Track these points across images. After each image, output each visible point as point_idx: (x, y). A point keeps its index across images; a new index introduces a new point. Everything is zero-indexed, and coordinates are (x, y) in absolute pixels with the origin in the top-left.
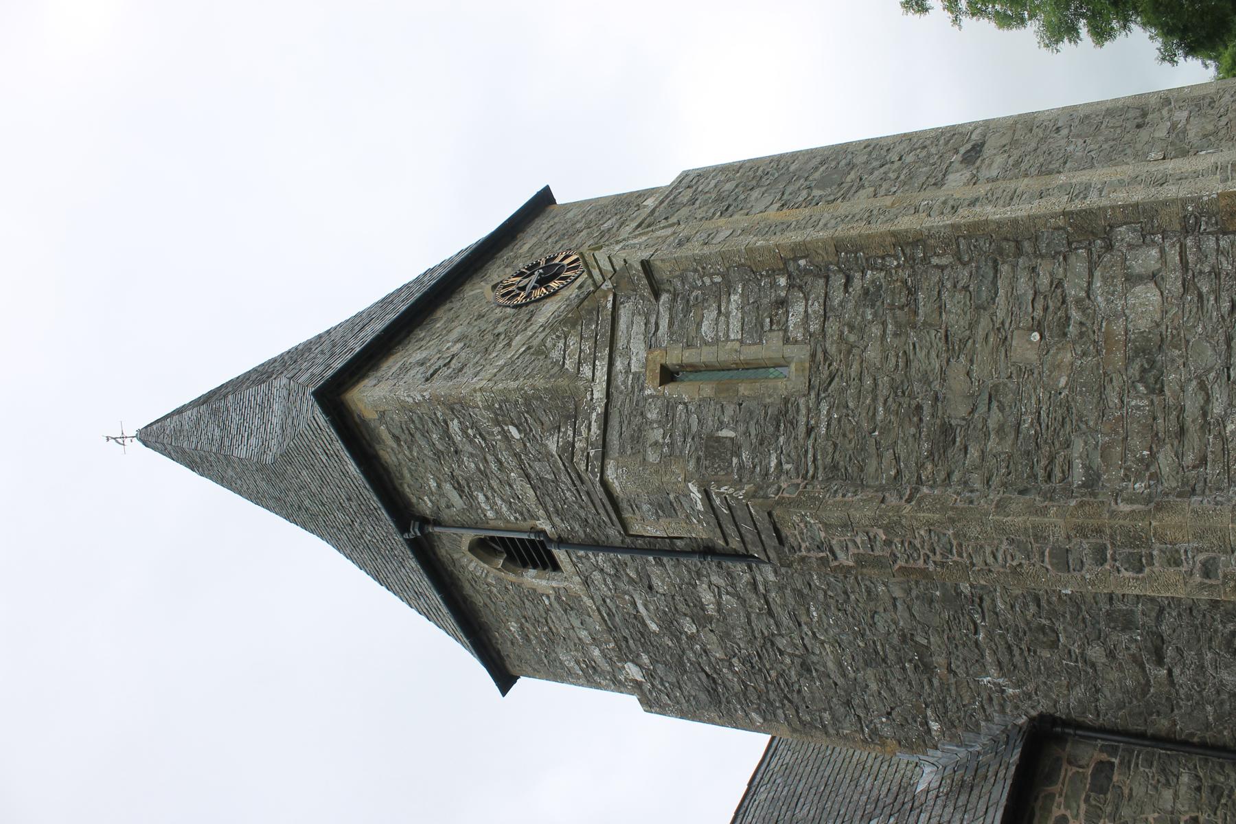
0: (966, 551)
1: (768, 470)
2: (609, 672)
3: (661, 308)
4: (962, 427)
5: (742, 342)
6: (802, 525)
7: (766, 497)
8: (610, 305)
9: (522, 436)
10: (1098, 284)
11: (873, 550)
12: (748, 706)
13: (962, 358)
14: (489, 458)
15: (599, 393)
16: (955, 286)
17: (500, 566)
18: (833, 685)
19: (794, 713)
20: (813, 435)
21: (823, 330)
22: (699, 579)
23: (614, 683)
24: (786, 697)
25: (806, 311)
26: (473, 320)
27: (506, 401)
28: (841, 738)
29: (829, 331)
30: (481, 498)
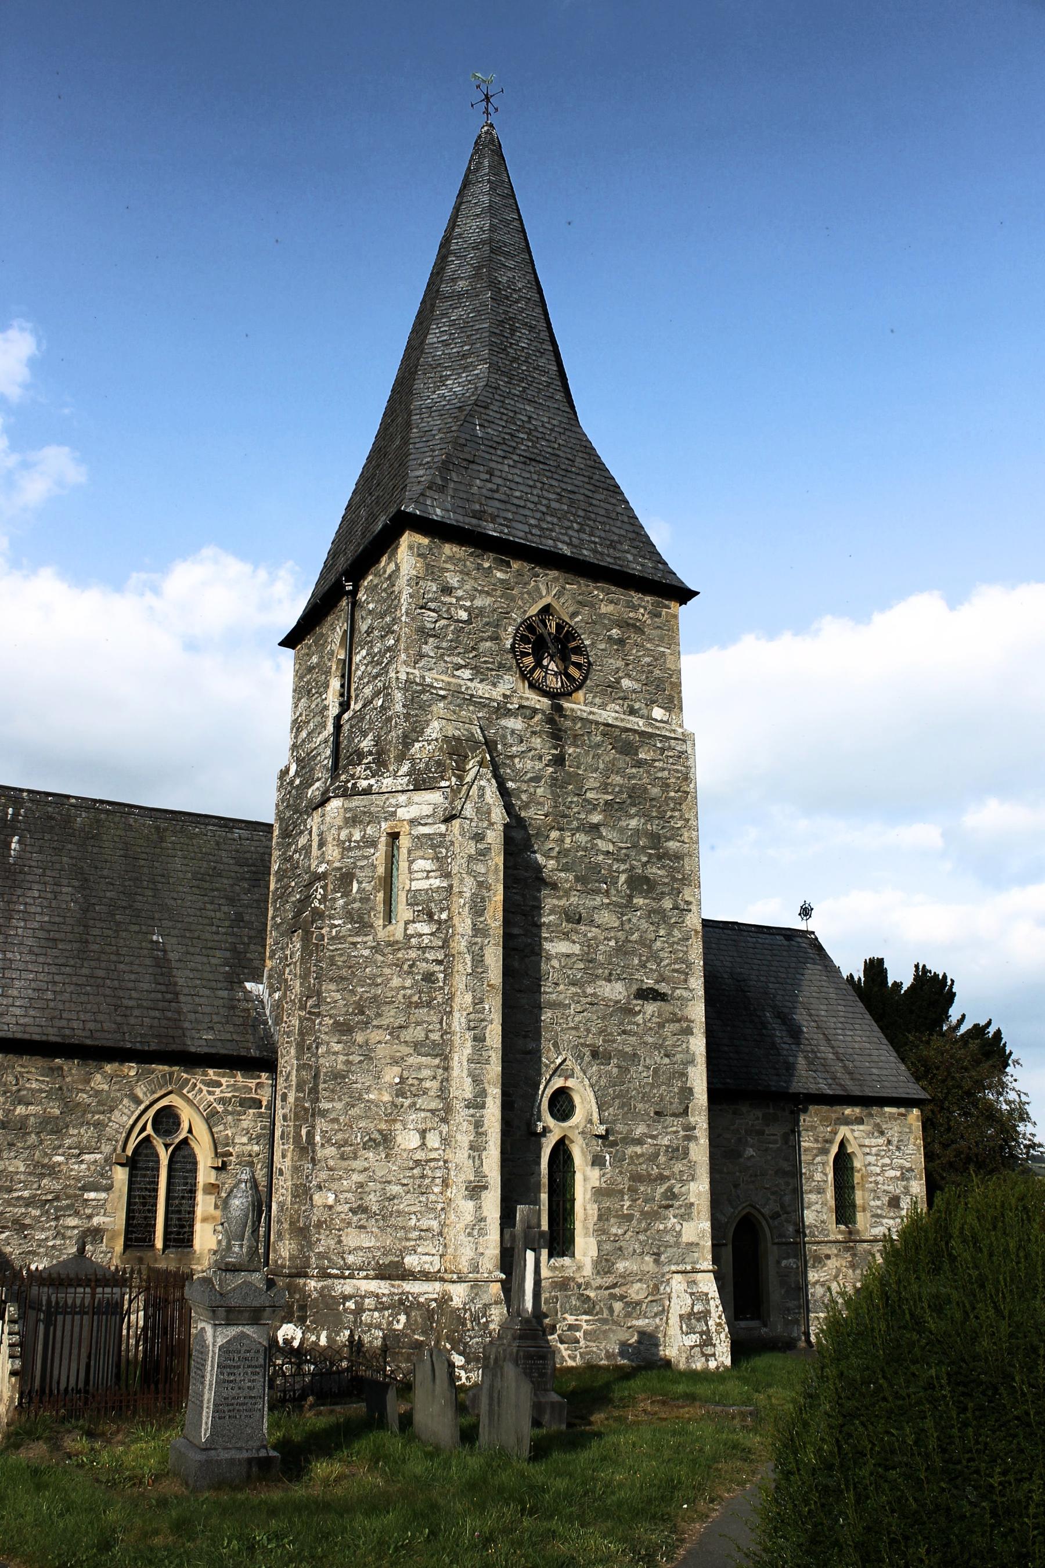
7: (312, 923)
10: (423, 1114)
13: (388, 1037)
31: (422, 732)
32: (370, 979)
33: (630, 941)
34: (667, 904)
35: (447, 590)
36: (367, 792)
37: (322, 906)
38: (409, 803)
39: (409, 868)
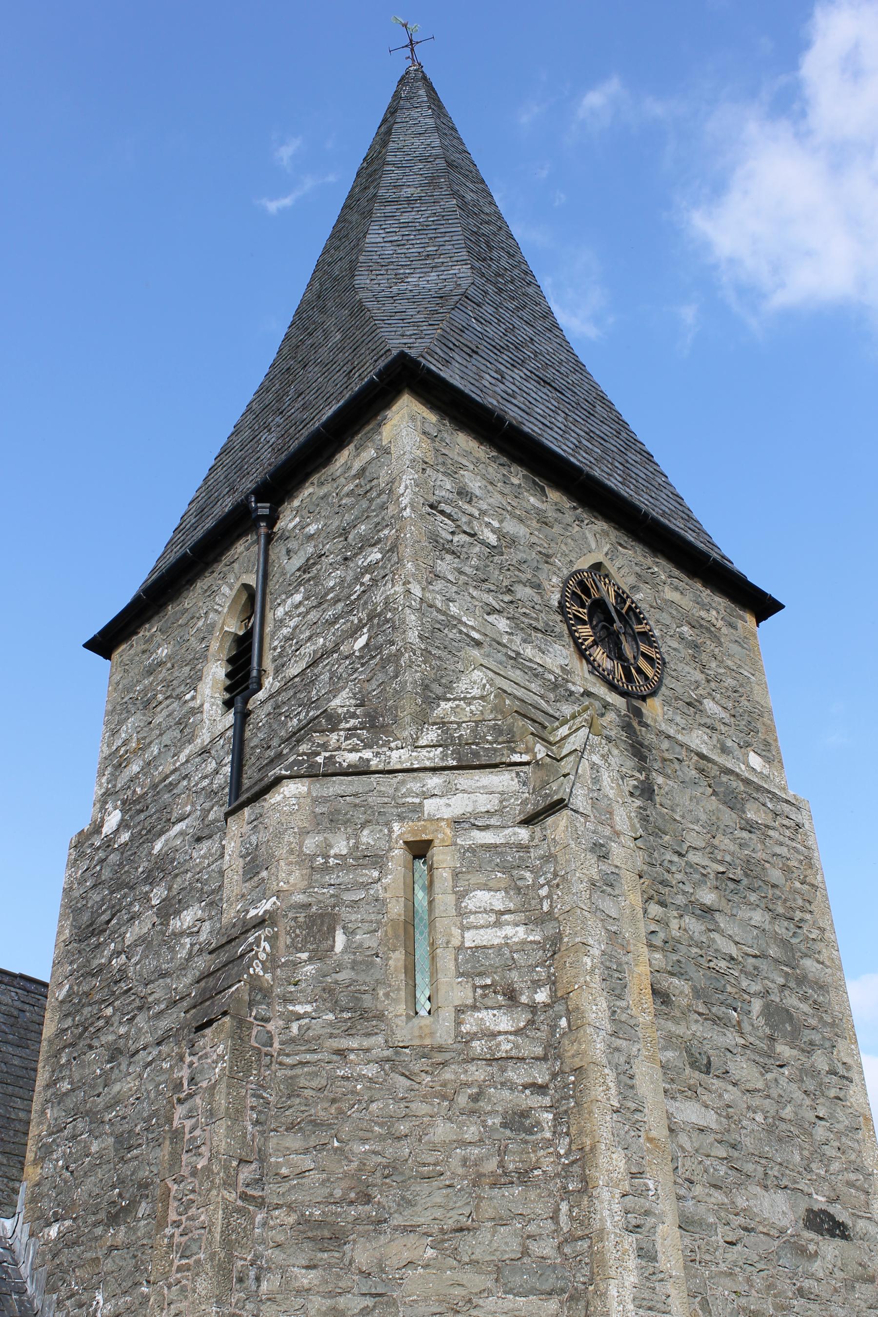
0: (182, 1277)
1: (292, 1002)
2: (114, 786)
3: (511, 829)
4: (341, 1259)
5: (460, 949)
6: (215, 1057)
7: (251, 1004)
8: (516, 758)
9: (357, 654)
11: (187, 1152)
12: (76, 979)
13: (430, 1253)
14: (340, 606)
15: (399, 757)
16: (529, 1237)
17: (226, 629)
18: (97, 1092)
19: (68, 1042)
20: (335, 1058)
21: (473, 1059)
22: (206, 905)
23: (105, 793)
24: (86, 1029)
25: (500, 1033)
26: (539, 549)
27: (394, 628)
28: (43, 1105)
29: (472, 1068)
30: (298, 598)
31: (449, 687)
32: (381, 1125)
33: (782, 1119)
34: (821, 1061)
35: (463, 493)
36: (361, 771)
37: (268, 976)
38: (449, 791)
39: (458, 906)
